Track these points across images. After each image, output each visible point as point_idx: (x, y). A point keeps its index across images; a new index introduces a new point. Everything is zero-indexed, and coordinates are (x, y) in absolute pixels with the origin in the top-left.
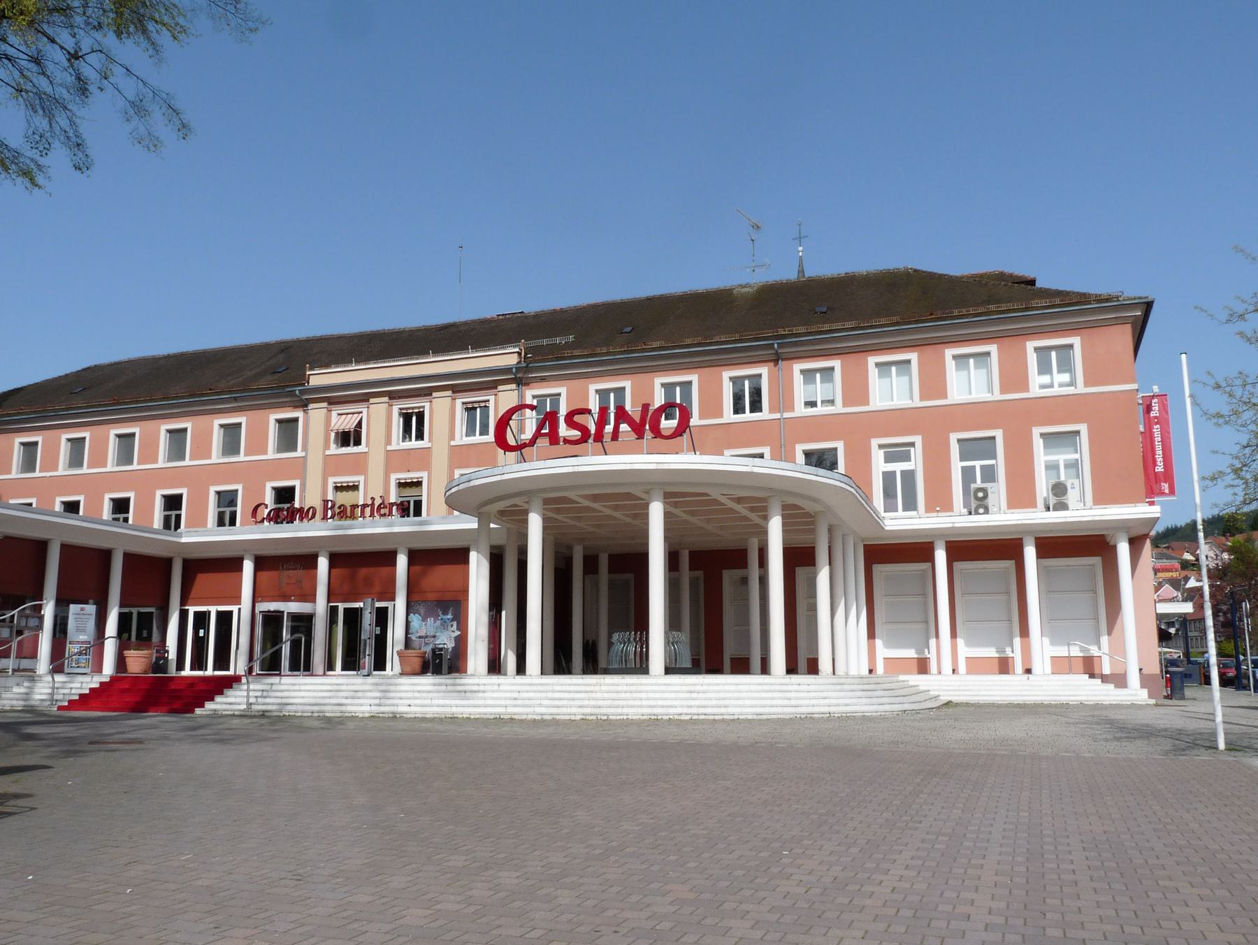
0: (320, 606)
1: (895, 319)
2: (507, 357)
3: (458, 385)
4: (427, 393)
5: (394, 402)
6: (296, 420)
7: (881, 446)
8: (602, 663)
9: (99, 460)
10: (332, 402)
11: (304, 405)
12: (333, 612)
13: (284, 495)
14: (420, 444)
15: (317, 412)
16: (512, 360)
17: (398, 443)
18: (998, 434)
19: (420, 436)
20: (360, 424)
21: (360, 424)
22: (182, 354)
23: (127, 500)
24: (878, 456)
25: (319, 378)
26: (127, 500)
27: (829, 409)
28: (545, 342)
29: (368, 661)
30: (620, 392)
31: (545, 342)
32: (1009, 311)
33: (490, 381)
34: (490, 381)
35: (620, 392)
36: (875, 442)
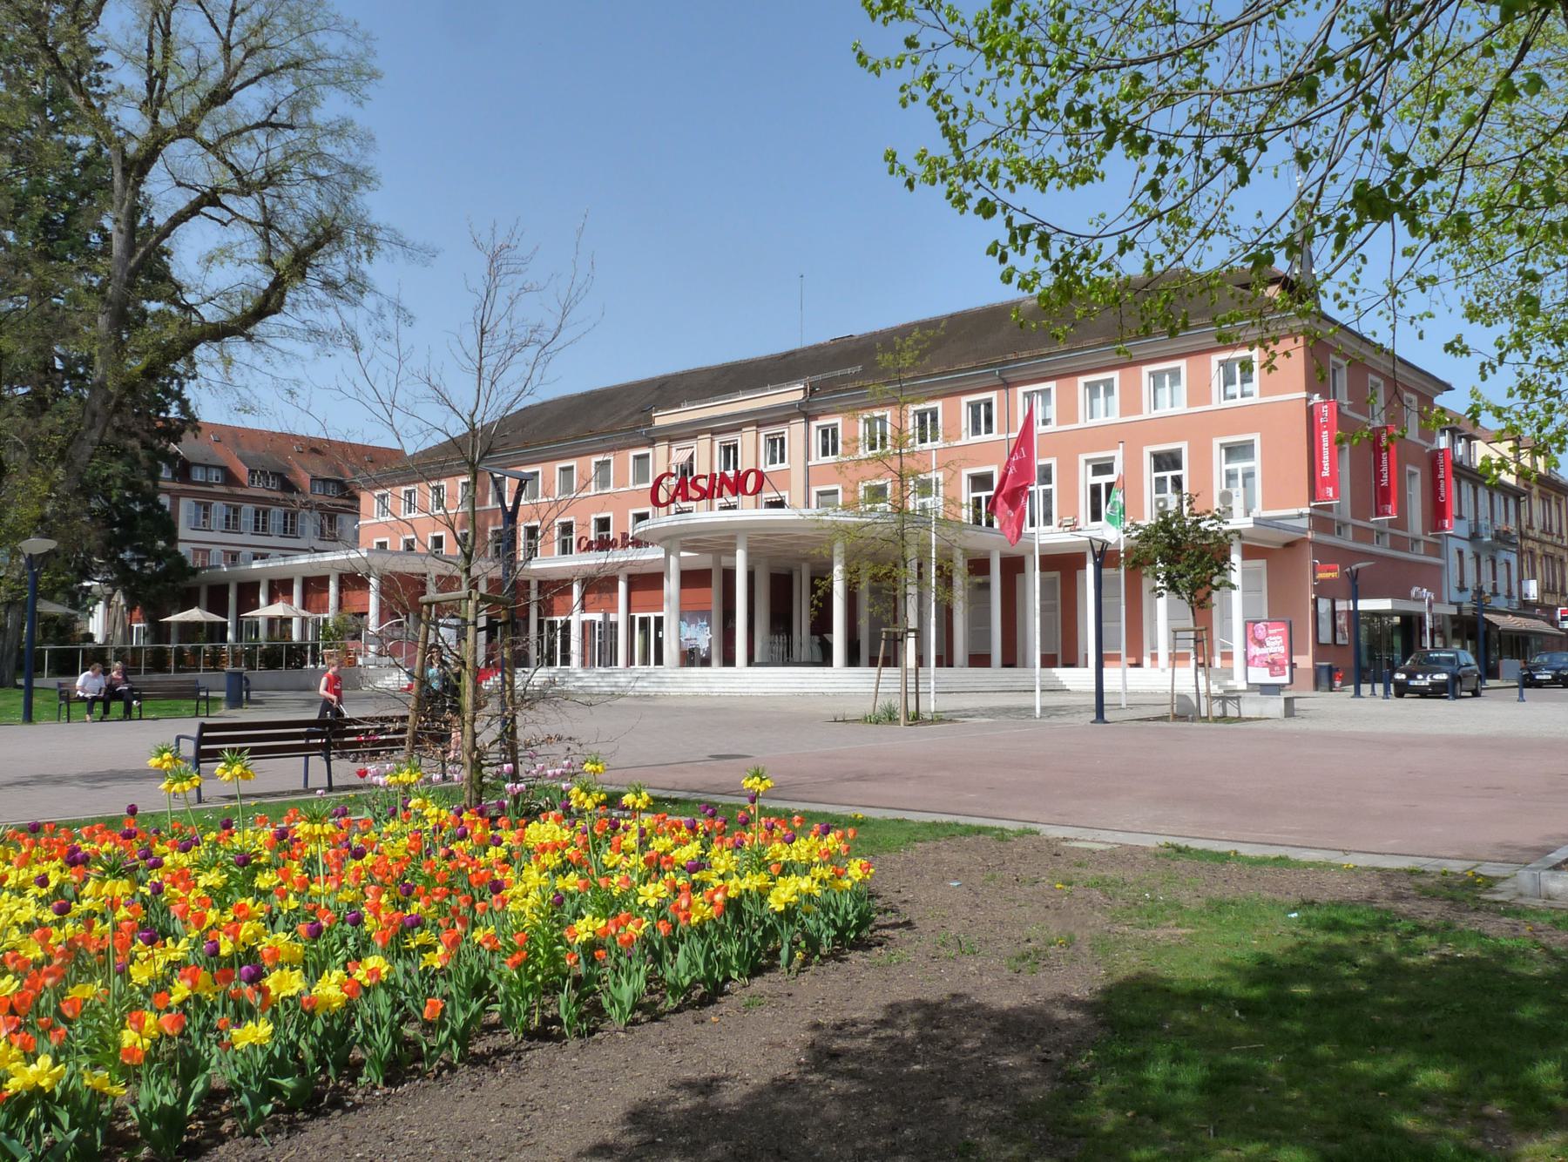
0: (620, 617)
1: (1101, 340)
2: (793, 394)
3: (760, 419)
4: (737, 429)
5: (675, 446)
6: (647, 456)
7: (1087, 461)
8: (796, 658)
9: (953, 434)
10: (672, 440)
11: (652, 443)
12: (631, 621)
13: (603, 524)
14: (989, 437)
15: (662, 448)
16: (799, 396)
17: (817, 459)
18: (1256, 438)
19: (782, 460)
20: (691, 457)
21: (691, 457)
22: (592, 392)
23: (607, 520)
24: (1218, 455)
25: (663, 419)
26: (607, 520)
27: (1247, 401)
28: (839, 373)
29: (1147, 660)
30: (883, 419)
31: (839, 373)
32: (1049, 355)
33: (783, 415)
34: (783, 415)
35: (883, 419)
36: (1082, 458)
